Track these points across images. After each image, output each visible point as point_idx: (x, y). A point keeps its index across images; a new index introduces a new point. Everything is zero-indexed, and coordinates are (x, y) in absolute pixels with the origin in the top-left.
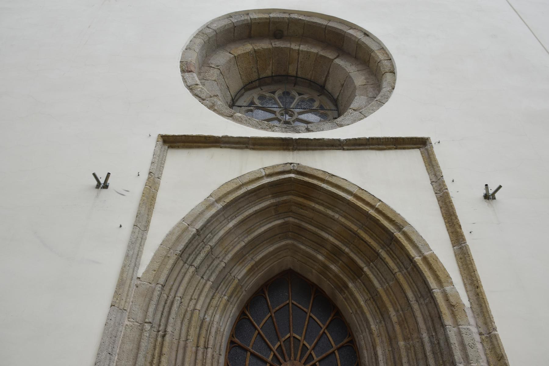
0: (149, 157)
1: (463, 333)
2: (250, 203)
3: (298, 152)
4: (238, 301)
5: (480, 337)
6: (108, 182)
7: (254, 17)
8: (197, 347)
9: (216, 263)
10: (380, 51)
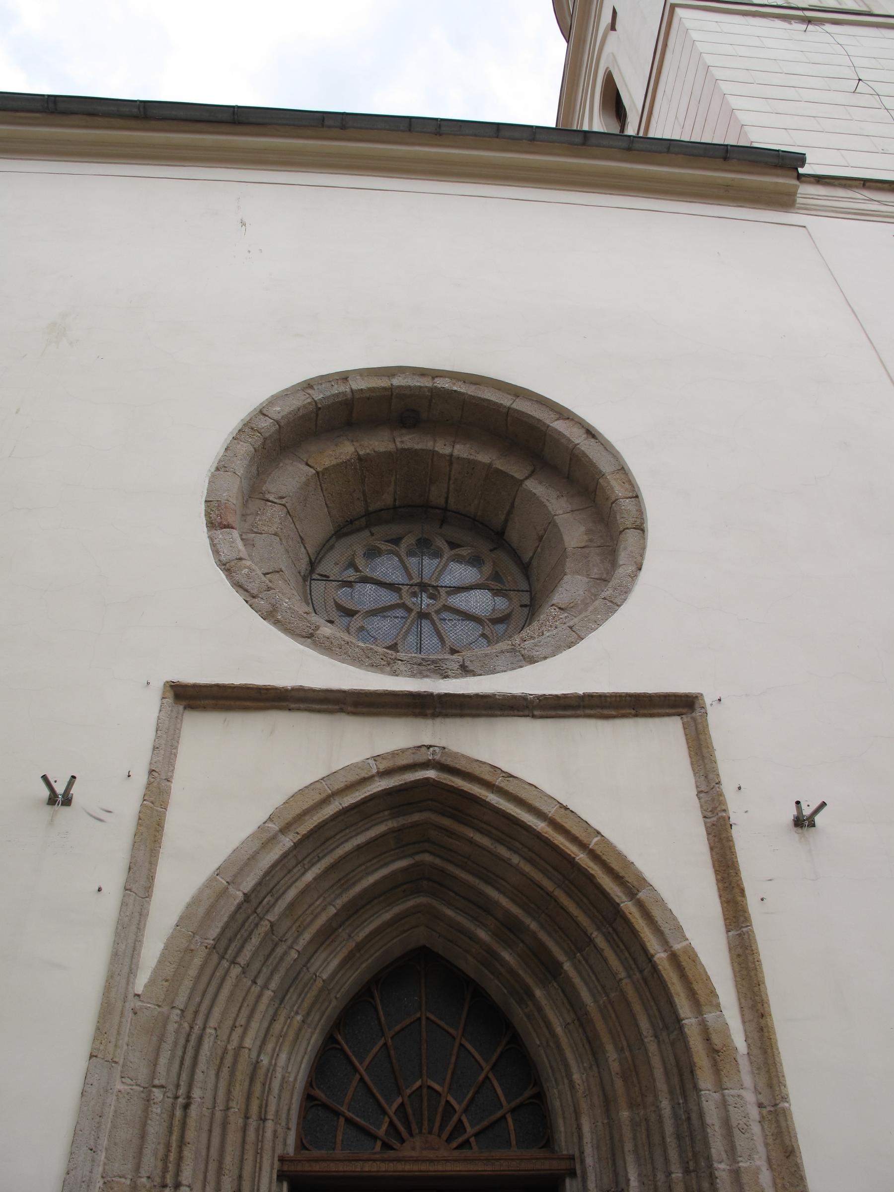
0: (146, 735)
1: (729, 1105)
2: (347, 828)
3: (443, 719)
4: (322, 1021)
5: (760, 1112)
6: (71, 793)
7: (360, 388)
8: (247, 1117)
9: (279, 951)
10: (618, 476)
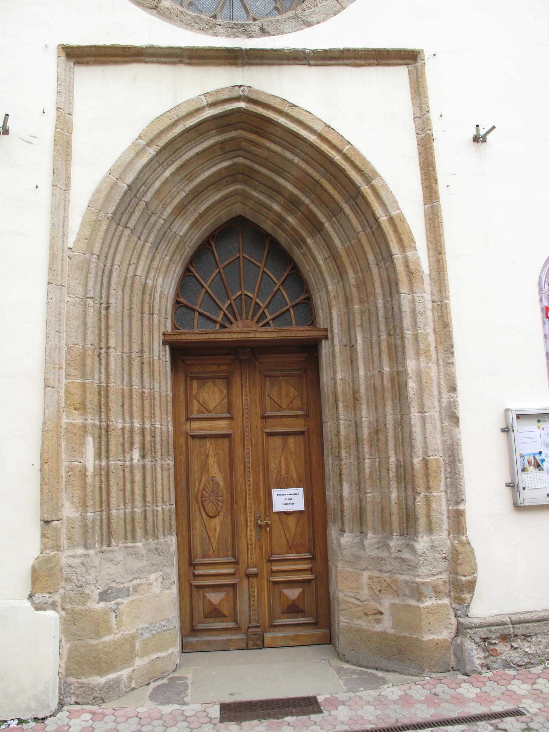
9: (153, 220)
